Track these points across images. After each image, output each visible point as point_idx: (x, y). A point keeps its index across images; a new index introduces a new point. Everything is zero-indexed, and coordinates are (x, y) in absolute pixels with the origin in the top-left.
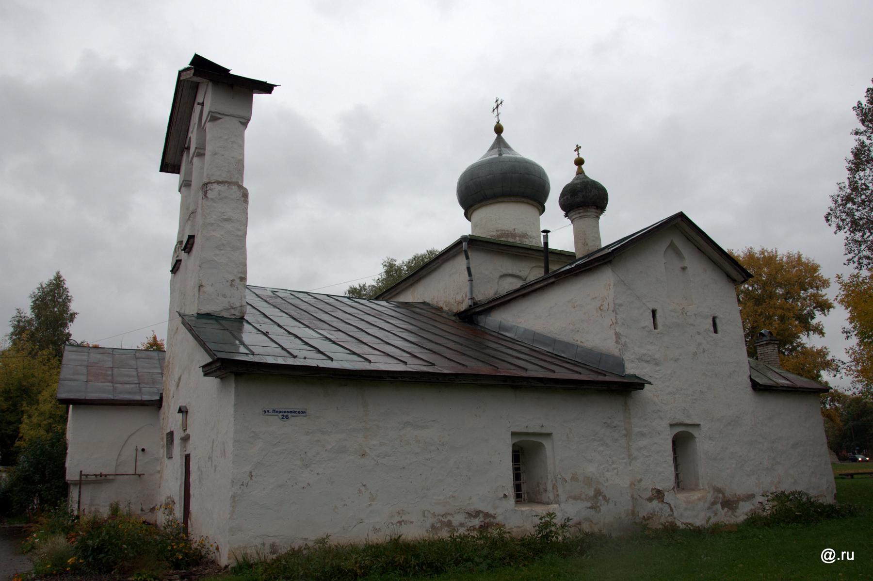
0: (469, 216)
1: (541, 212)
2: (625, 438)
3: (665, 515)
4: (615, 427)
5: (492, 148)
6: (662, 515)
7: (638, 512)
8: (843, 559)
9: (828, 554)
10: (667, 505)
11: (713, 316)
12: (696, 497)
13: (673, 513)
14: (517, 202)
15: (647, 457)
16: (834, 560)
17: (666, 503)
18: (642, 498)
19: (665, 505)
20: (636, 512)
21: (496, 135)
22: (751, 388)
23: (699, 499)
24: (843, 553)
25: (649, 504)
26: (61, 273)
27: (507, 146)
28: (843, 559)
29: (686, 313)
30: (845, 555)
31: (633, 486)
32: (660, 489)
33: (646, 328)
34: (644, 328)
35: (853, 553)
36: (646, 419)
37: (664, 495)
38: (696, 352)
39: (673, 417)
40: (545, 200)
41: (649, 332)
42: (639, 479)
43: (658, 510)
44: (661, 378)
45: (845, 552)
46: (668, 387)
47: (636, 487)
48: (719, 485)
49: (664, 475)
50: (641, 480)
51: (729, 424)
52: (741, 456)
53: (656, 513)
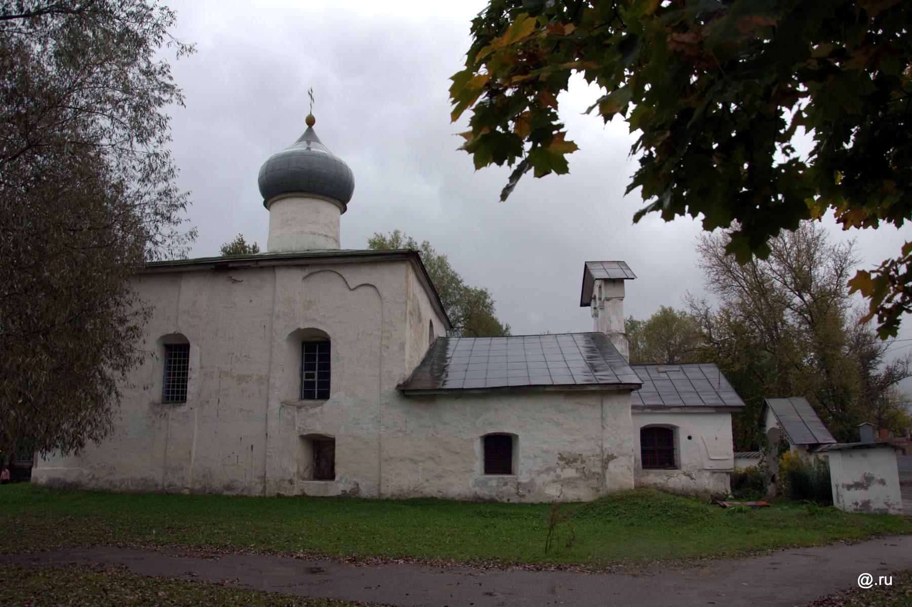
0: (268, 205)
1: (343, 210)
5: (301, 140)
8: (880, 584)
9: (865, 579)
14: (323, 199)
21: (307, 126)
24: (881, 578)
26: (566, 91)
27: (316, 140)
28: (880, 584)
35: (891, 577)
40: (348, 199)
45: (883, 577)
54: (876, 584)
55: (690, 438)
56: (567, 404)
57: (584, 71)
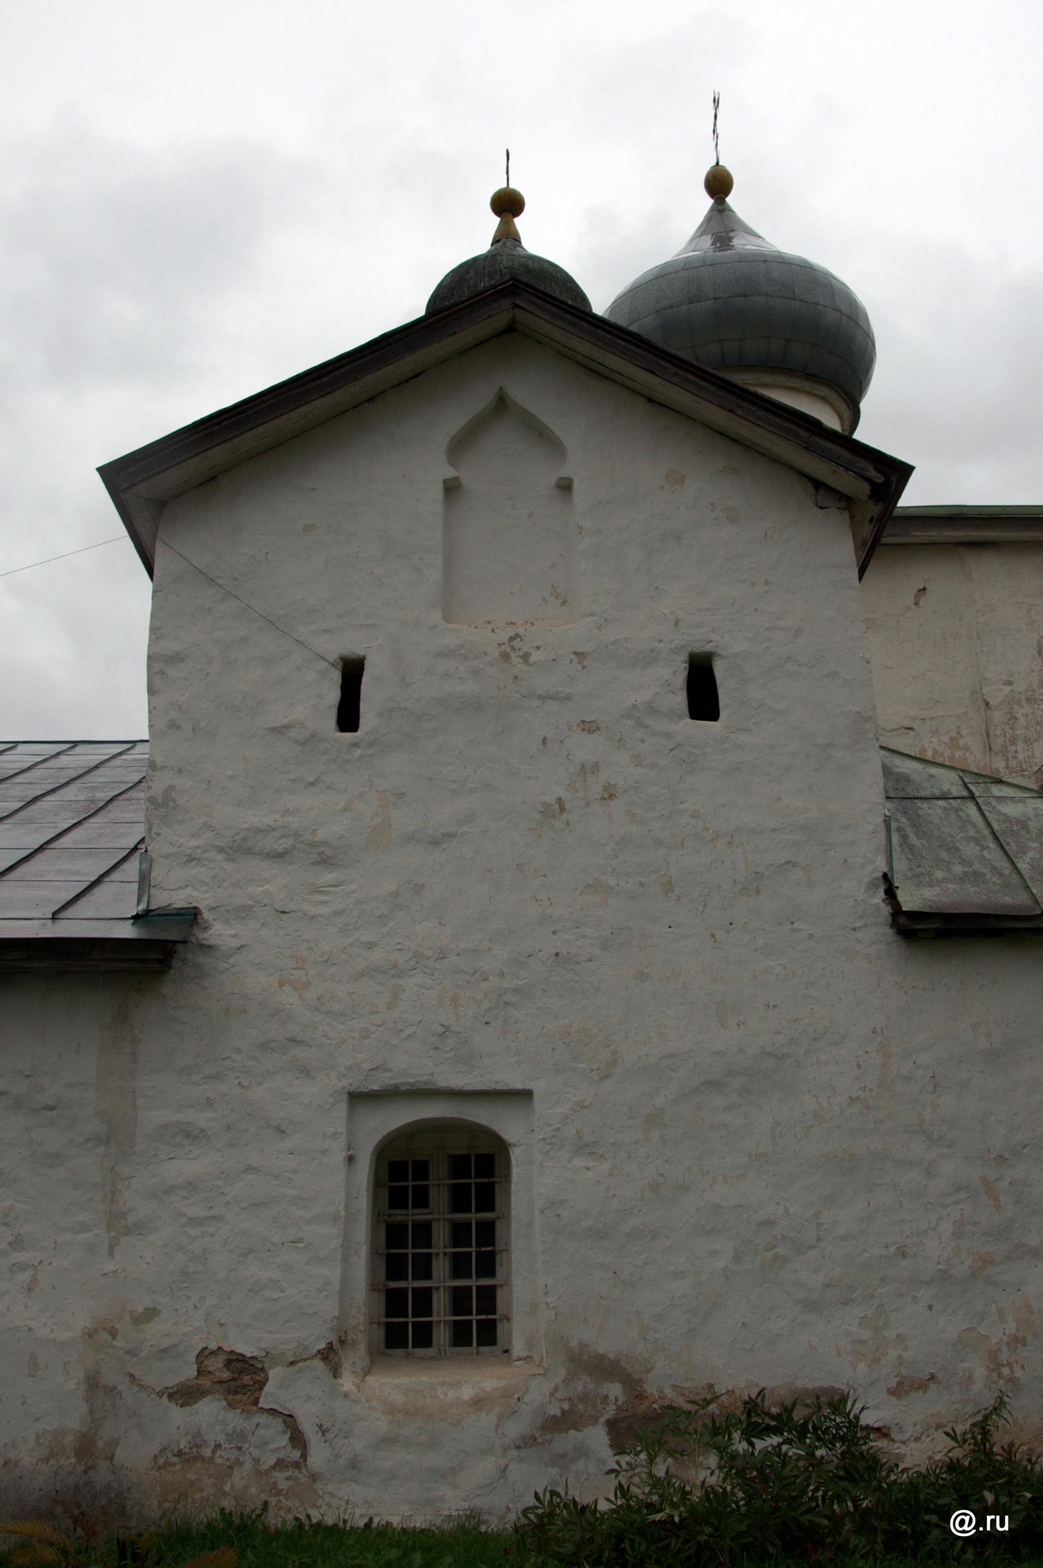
2: (101, 1149)
3: (257, 1461)
4: (52, 1108)
6: (238, 1462)
7: (114, 1443)
8: (988, 1529)
10: (277, 1423)
11: (689, 649)
12: (467, 1393)
13: (304, 1456)
15: (193, 1221)
16: (974, 1531)
17: (272, 1411)
18: (142, 1387)
19: (262, 1418)
20: (100, 1444)
22: (889, 931)
23: (478, 1403)
24: (989, 1518)
25: (178, 1415)
28: (988, 1529)
29: (526, 657)
30: (993, 1522)
31: (104, 1336)
32: (249, 1354)
33: (293, 733)
34: (278, 731)
35: (1007, 1517)
36: (217, 1077)
37: (267, 1379)
38: (559, 800)
39: (367, 1066)
41: (304, 743)
42: (140, 1309)
43: (221, 1438)
44: (338, 913)
45: (993, 1517)
46: (371, 946)
47: (119, 1343)
48: (607, 1346)
49: (276, 1295)
50: (151, 1314)
51: (714, 1085)
52: (769, 1223)
53: (207, 1452)
54: (981, 1529)
55: (731, 924)
56: (115, 921)
57: (901, 503)
